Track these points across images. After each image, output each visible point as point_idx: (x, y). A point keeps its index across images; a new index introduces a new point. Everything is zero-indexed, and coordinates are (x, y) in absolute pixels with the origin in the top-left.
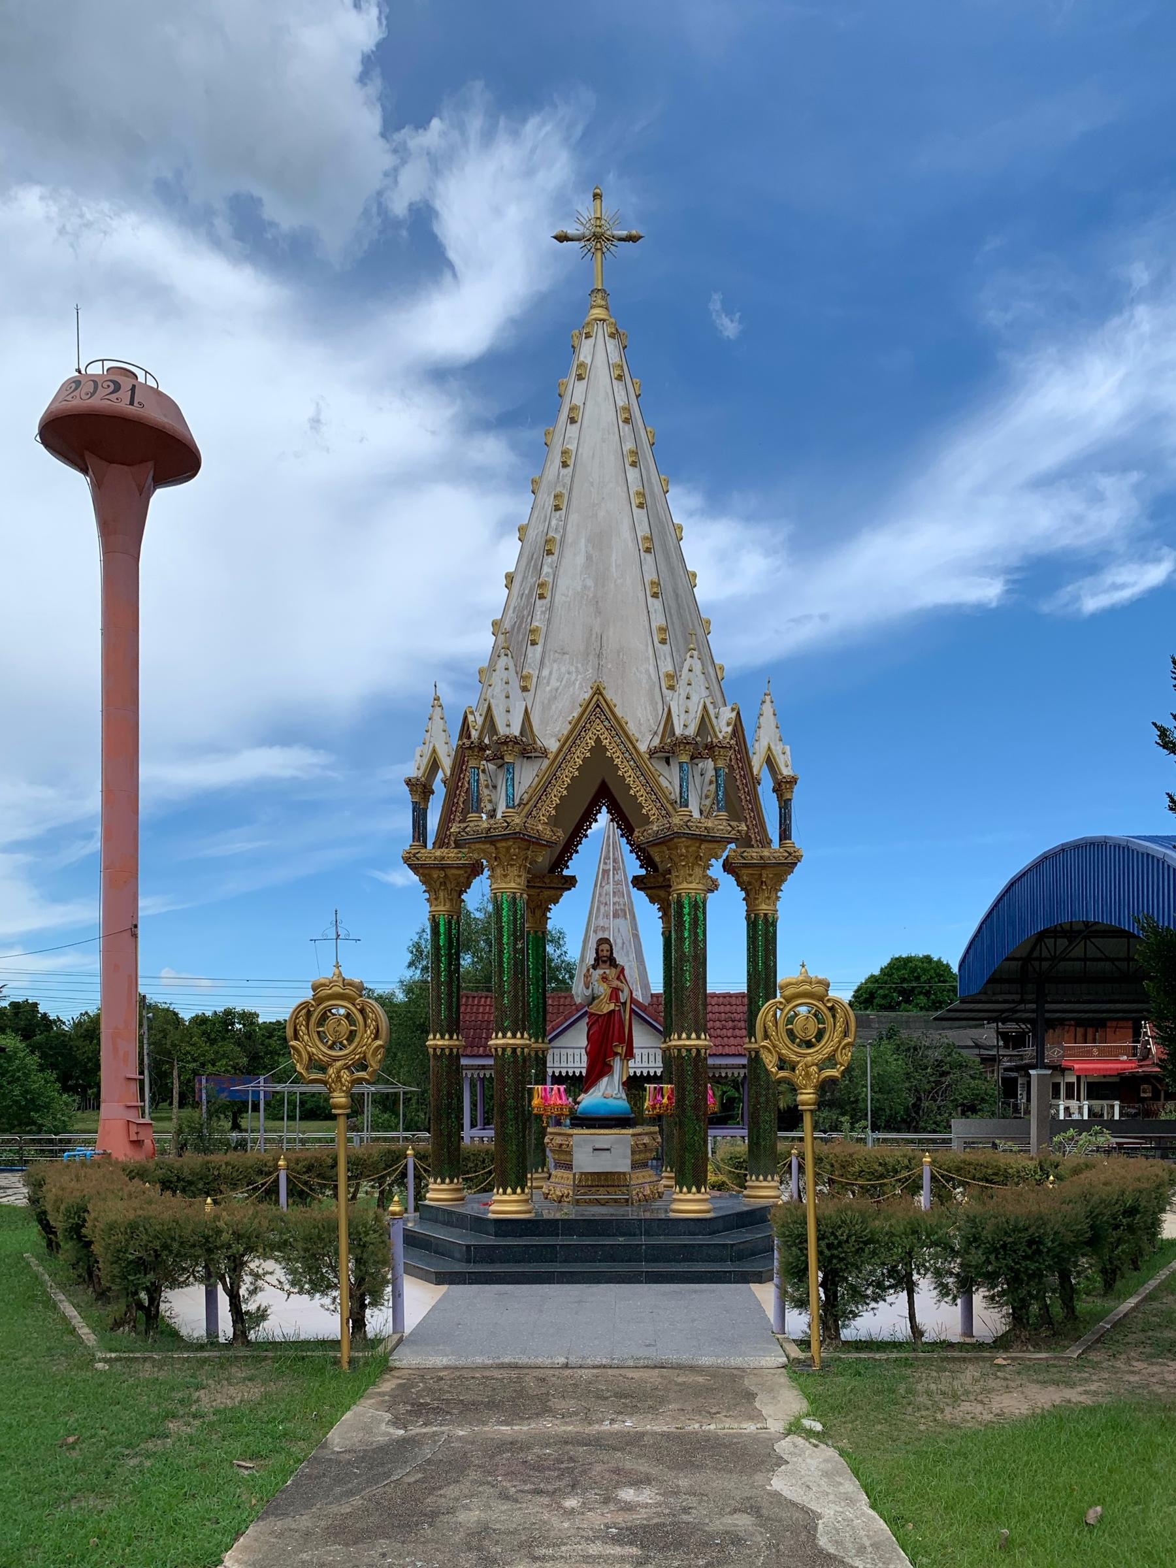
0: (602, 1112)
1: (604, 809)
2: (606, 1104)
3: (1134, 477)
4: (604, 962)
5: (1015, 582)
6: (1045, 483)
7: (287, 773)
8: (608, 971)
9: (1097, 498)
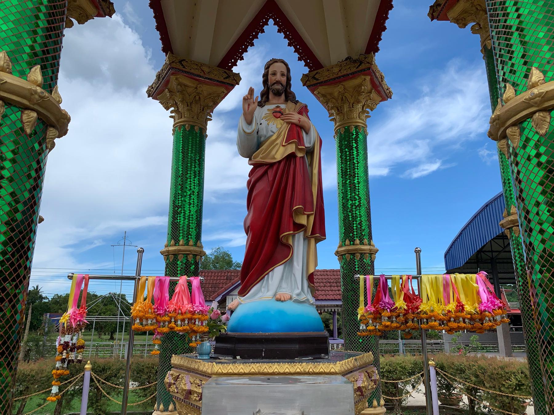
0: (274, 328)
1: (271, 22)
2: (281, 313)
3: (428, 141)
4: (278, 94)
5: (392, 169)
6: (400, 142)
7: (160, 224)
8: (283, 106)
9: (416, 146)
